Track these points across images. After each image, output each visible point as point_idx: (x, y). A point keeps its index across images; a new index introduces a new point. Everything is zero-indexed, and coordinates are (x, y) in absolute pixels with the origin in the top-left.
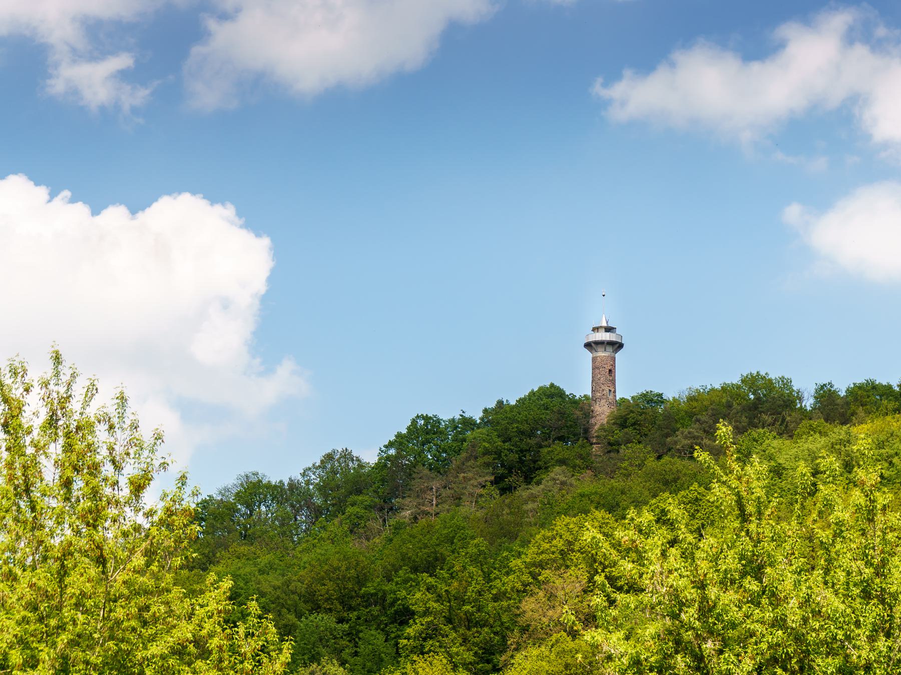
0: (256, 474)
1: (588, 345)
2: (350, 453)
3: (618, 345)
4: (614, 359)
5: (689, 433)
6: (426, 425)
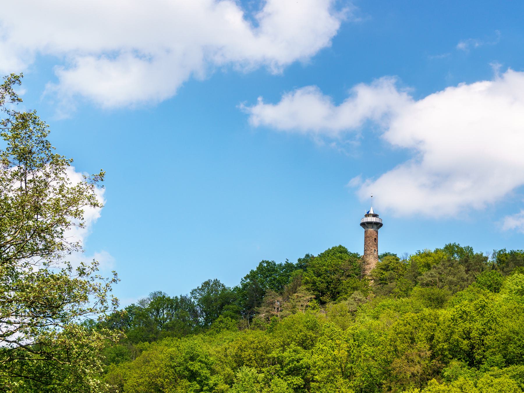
0: (161, 293)
1: (363, 225)
2: (219, 282)
3: (380, 225)
4: (377, 232)
5: (431, 274)
6: (268, 265)
